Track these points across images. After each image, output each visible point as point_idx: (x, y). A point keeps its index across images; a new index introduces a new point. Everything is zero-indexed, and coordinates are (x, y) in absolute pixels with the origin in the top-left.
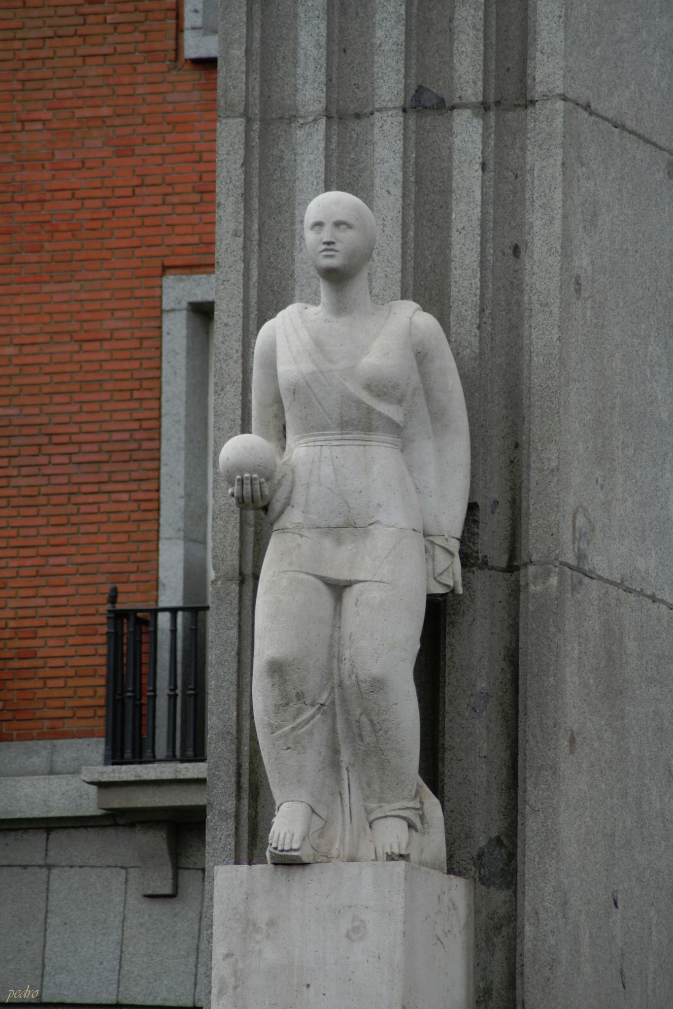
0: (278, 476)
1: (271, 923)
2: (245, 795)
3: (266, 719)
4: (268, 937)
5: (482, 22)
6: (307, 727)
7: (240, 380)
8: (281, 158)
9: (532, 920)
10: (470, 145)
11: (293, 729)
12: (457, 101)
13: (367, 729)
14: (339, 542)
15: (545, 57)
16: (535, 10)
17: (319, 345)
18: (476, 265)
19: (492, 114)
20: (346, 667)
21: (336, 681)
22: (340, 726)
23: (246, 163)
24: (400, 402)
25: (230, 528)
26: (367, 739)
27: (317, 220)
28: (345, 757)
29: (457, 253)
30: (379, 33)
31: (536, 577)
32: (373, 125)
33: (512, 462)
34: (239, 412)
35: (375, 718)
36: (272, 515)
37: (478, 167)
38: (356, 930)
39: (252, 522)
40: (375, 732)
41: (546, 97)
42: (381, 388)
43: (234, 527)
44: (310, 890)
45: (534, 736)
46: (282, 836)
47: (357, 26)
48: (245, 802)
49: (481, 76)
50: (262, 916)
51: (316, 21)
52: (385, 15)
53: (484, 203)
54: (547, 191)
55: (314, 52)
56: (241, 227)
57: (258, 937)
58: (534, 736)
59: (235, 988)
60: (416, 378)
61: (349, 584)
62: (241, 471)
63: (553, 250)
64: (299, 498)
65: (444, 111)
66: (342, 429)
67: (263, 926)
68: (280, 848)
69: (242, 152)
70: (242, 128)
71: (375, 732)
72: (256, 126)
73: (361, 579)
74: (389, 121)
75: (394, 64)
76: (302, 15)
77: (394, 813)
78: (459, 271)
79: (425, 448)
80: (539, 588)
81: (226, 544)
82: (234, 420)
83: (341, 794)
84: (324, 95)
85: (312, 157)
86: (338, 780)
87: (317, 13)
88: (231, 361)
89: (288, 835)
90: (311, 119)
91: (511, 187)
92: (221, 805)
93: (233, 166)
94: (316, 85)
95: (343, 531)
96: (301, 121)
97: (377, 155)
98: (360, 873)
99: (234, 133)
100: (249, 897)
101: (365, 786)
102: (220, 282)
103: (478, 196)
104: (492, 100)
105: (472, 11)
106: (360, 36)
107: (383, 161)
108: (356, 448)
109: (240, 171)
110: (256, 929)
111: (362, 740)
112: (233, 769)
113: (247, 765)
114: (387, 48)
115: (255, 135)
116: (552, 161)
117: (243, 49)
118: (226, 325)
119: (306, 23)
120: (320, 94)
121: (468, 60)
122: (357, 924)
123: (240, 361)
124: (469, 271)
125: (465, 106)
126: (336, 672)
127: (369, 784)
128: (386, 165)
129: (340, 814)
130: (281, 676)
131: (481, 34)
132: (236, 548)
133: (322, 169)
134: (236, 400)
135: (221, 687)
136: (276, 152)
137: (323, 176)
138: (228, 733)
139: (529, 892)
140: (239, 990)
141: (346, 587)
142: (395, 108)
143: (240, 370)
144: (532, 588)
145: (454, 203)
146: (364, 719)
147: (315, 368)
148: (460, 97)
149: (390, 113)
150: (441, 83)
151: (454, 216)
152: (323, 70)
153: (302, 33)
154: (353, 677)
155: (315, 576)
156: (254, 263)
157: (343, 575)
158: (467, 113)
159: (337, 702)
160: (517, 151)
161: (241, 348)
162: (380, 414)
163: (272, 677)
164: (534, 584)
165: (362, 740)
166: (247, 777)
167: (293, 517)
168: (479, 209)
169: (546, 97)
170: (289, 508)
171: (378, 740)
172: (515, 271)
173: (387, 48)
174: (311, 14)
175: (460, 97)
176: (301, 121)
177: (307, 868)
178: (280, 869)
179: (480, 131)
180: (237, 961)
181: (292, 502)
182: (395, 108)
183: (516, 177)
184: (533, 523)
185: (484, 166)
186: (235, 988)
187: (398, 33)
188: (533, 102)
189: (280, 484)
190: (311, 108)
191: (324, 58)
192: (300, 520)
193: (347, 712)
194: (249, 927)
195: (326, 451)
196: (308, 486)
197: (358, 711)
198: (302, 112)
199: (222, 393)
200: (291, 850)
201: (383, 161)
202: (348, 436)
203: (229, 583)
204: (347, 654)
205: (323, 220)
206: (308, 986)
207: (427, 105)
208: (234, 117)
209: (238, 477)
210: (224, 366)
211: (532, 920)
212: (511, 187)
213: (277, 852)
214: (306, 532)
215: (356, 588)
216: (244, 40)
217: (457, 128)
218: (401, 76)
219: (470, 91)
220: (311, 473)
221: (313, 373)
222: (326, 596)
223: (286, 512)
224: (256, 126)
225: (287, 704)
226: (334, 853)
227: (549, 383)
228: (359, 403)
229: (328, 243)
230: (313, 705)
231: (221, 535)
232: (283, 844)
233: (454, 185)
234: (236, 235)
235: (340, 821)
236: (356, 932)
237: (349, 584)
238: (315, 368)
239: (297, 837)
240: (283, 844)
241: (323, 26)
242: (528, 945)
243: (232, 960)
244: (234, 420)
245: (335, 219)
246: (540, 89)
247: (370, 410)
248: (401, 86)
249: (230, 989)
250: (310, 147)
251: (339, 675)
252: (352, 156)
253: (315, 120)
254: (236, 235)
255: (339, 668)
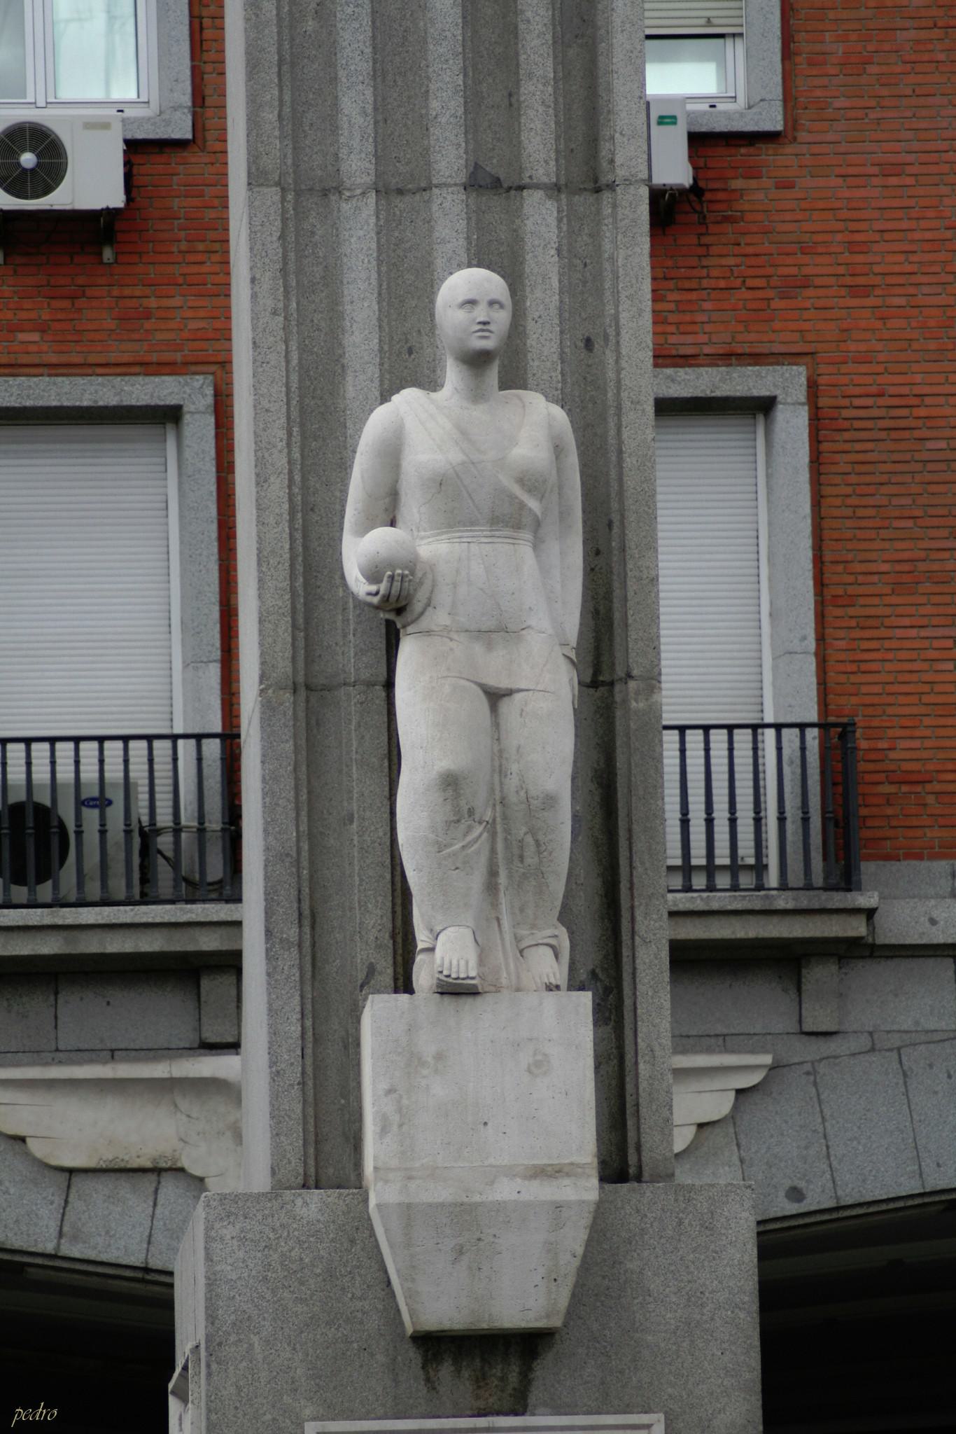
0: (419, 574)
1: (439, 1057)
2: (307, 922)
3: (432, 836)
4: (436, 1071)
5: (552, 98)
6: (476, 846)
7: (286, 471)
8: (313, 233)
9: (647, 1058)
10: (543, 229)
11: (463, 847)
12: (528, 180)
13: (530, 851)
14: (490, 647)
15: (625, 139)
16: (609, 90)
17: (463, 433)
18: (555, 357)
19: (563, 196)
20: (512, 782)
21: (498, 798)
22: (500, 846)
23: (282, 237)
24: (541, 499)
25: (280, 631)
26: (528, 861)
27: (470, 297)
28: (502, 879)
29: (534, 343)
30: (435, 104)
31: (637, 693)
32: (429, 201)
33: (592, 570)
34: (286, 506)
35: (540, 837)
36: (408, 616)
37: (553, 252)
38: (538, 1064)
39: (302, 627)
40: (540, 853)
41: (628, 182)
42: (531, 482)
43: (286, 630)
44: (479, 1023)
45: (642, 863)
46: (455, 963)
47: (395, 95)
48: (307, 929)
49: (553, 156)
50: (427, 1045)
51: (360, 87)
52: (440, 84)
53: (561, 292)
54: (634, 281)
55: (359, 120)
56: (281, 305)
57: (425, 1072)
58: (642, 863)
59: (401, 1126)
60: (554, 472)
61: (510, 693)
62: (392, 566)
63: (644, 345)
64: (443, 597)
65: (501, 191)
66: (492, 524)
67: (429, 1059)
68: (454, 976)
69: (278, 223)
70: (277, 198)
71: (540, 853)
72: (290, 197)
73: (523, 687)
74: (449, 198)
75: (452, 138)
76: (344, 80)
77: (545, 941)
78: (536, 363)
79: (553, 548)
80: (641, 705)
81: (277, 649)
82: (281, 515)
83: (498, 919)
84: (373, 167)
85: (361, 233)
86: (495, 905)
87: (361, 78)
88: (275, 451)
89: (462, 963)
90: (358, 191)
91: (579, 276)
92: (282, 933)
93: (269, 239)
94: (363, 155)
95: (494, 636)
96: (348, 194)
97: (437, 234)
98: (541, 1004)
99: (269, 203)
100: (411, 1029)
101: (517, 911)
102: (258, 364)
103: (555, 284)
104: (563, 181)
105: (540, 86)
106: (399, 106)
107: (443, 242)
108: (507, 547)
109: (276, 245)
110: (422, 1063)
111: (522, 861)
112: (294, 893)
113: (307, 890)
114: (444, 120)
115: (290, 206)
116: (637, 249)
117: (276, 112)
118: (267, 411)
119: (349, 88)
120: (368, 165)
121: (538, 138)
122: (539, 1057)
123: (286, 450)
124: (548, 364)
125: (537, 187)
126: (497, 787)
127: (522, 910)
128: (449, 246)
129: (499, 941)
130: (455, 790)
131: (551, 111)
132: (288, 654)
133: (374, 246)
134: (281, 494)
135: (277, 804)
136: (306, 226)
137: (375, 255)
138: (287, 855)
139: (643, 1029)
140: (405, 1128)
141: (504, 695)
142: (456, 185)
143: (285, 460)
144: (634, 704)
145: (528, 289)
146: (529, 839)
147: (464, 458)
148: (530, 177)
149: (450, 190)
150: (495, 161)
151: (528, 304)
152: (371, 140)
153: (345, 99)
154: (522, 793)
155: (476, 683)
156: (294, 346)
157: (503, 683)
158: (539, 194)
159: (498, 820)
160: (585, 238)
161: (285, 437)
162: (530, 509)
163: (444, 790)
164: (636, 701)
165: (522, 861)
166: (307, 903)
167: (438, 618)
168: (557, 297)
169: (628, 182)
170: (430, 609)
171: (541, 862)
172: (589, 366)
173: (444, 120)
174: (354, 79)
175: (530, 177)
176: (348, 194)
177: (479, 999)
178: (447, 999)
179: (555, 214)
180: (401, 1097)
181: (433, 603)
182: (456, 185)
183: (585, 265)
184: (633, 635)
185: (559, 251)
186: (401, 1126)
187: (456, 105)
188: (611, 187)
189: (421, 583)
190: (359, 181)
191: (371, 126)
192: (448, 623)
193: (507, 831)
194: (413, 1061)
195: (474, 548)
196: (455, 585)
197: (524, 829)
198: (348, 183)
199: (266, 485)
200: (468, 978)
201: (443, 242)
202: (497, 533)
203: (281, 692)
204: (514, 768)
205: (477, 298)
206: (485, 1124)
207: (482, 183)
208: (268, 186)
209: (389, 573)
210: (266, 455)
211: (647, 1058)
212: (579, 276)
213: (450, 980)
214: (455, 636)
215: (517, 696)
216: (277, 103)
217: (527, 209)
218: (462, 151)
219: (541, 171)
220: (458, 571)
221: (463, 463)
222: (483, 704)
223: (427, 613)
224: (290, 197)
225: (458, 821)
226: (504, 981)
227: (644, 485)
228: (512, 497)
229: (485, 323)
230: (480, 823)
231: (270, 640)
232: (458, 972)
233: (527, 270)
234: (275, 313)
235: (500, 948)
236: (539, 1066)
237: (510, 693)
238: (464, 458)
239: (473, 962)
240: (458, 972)
241: (369, 93)
242: (643, 1085)
243: (394, 1096)
244: (281, 515)
245: (489, 298)
246: (621, 173)
247: (522, 506)
248: (462, 162)
249: (395, 1128)
250: (449, 215)
251: (502, 791)
252: (396, 234)
253: (363, 193)
254: (275, 313)
255: (501, 783)
